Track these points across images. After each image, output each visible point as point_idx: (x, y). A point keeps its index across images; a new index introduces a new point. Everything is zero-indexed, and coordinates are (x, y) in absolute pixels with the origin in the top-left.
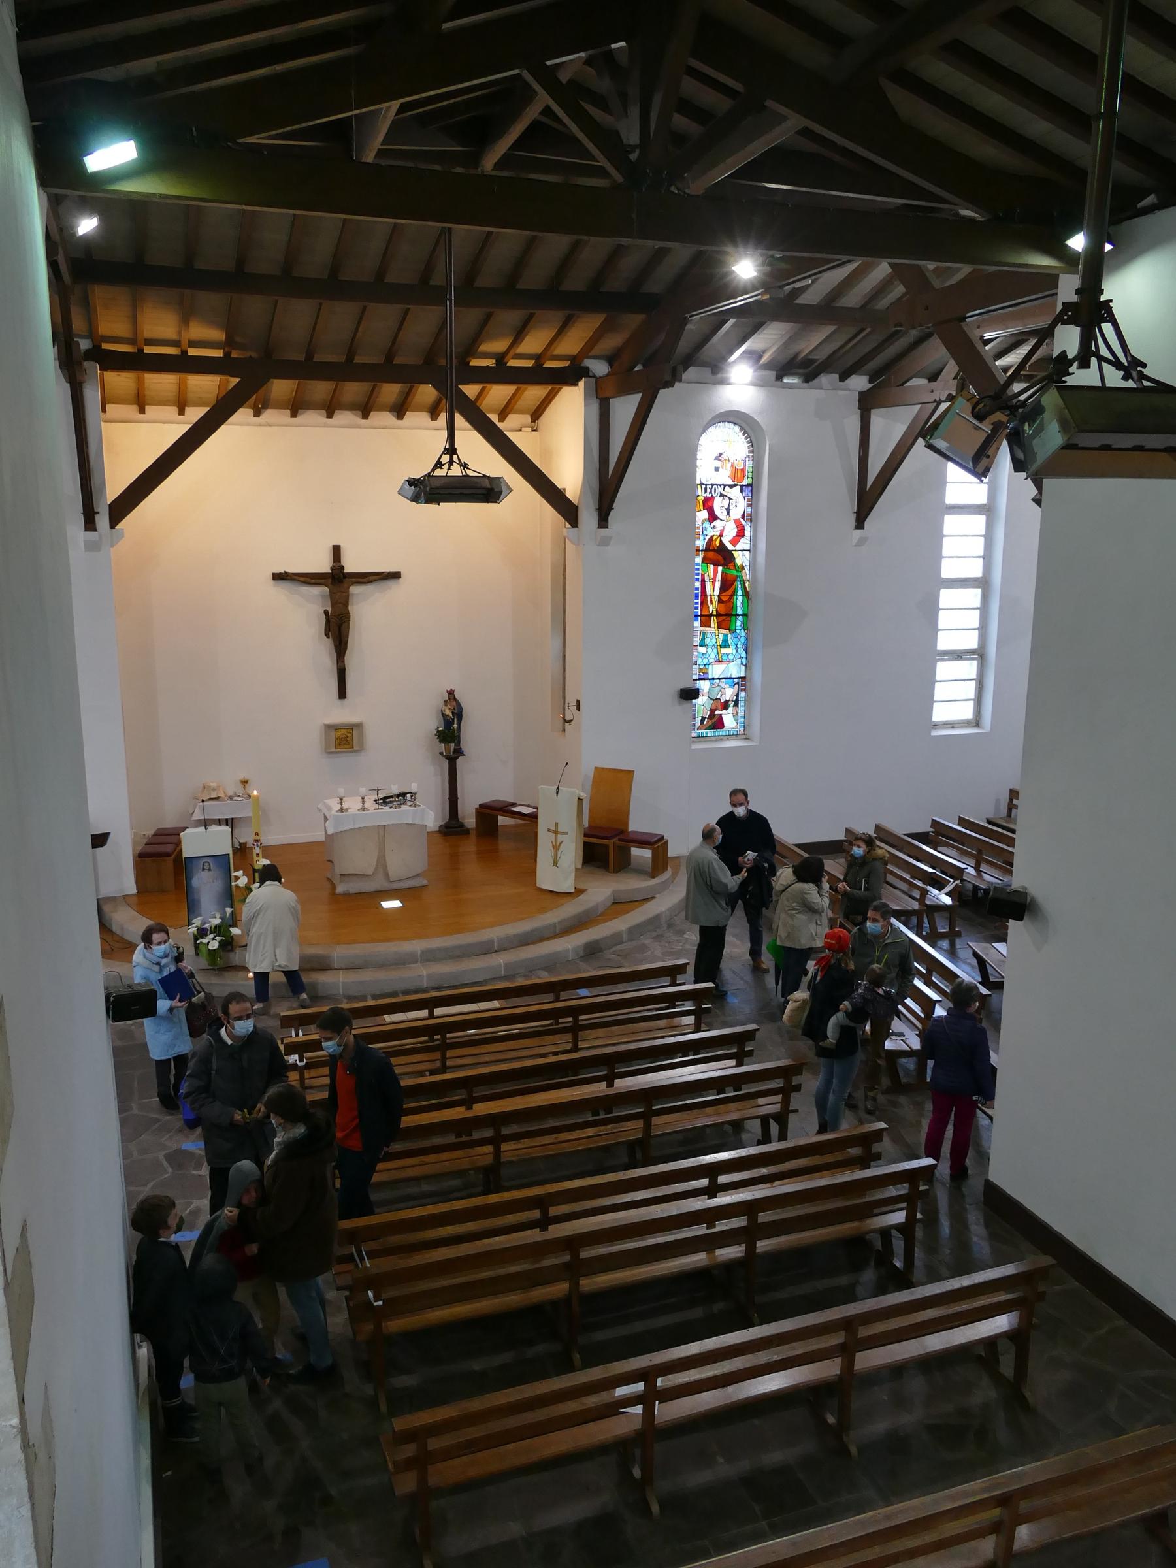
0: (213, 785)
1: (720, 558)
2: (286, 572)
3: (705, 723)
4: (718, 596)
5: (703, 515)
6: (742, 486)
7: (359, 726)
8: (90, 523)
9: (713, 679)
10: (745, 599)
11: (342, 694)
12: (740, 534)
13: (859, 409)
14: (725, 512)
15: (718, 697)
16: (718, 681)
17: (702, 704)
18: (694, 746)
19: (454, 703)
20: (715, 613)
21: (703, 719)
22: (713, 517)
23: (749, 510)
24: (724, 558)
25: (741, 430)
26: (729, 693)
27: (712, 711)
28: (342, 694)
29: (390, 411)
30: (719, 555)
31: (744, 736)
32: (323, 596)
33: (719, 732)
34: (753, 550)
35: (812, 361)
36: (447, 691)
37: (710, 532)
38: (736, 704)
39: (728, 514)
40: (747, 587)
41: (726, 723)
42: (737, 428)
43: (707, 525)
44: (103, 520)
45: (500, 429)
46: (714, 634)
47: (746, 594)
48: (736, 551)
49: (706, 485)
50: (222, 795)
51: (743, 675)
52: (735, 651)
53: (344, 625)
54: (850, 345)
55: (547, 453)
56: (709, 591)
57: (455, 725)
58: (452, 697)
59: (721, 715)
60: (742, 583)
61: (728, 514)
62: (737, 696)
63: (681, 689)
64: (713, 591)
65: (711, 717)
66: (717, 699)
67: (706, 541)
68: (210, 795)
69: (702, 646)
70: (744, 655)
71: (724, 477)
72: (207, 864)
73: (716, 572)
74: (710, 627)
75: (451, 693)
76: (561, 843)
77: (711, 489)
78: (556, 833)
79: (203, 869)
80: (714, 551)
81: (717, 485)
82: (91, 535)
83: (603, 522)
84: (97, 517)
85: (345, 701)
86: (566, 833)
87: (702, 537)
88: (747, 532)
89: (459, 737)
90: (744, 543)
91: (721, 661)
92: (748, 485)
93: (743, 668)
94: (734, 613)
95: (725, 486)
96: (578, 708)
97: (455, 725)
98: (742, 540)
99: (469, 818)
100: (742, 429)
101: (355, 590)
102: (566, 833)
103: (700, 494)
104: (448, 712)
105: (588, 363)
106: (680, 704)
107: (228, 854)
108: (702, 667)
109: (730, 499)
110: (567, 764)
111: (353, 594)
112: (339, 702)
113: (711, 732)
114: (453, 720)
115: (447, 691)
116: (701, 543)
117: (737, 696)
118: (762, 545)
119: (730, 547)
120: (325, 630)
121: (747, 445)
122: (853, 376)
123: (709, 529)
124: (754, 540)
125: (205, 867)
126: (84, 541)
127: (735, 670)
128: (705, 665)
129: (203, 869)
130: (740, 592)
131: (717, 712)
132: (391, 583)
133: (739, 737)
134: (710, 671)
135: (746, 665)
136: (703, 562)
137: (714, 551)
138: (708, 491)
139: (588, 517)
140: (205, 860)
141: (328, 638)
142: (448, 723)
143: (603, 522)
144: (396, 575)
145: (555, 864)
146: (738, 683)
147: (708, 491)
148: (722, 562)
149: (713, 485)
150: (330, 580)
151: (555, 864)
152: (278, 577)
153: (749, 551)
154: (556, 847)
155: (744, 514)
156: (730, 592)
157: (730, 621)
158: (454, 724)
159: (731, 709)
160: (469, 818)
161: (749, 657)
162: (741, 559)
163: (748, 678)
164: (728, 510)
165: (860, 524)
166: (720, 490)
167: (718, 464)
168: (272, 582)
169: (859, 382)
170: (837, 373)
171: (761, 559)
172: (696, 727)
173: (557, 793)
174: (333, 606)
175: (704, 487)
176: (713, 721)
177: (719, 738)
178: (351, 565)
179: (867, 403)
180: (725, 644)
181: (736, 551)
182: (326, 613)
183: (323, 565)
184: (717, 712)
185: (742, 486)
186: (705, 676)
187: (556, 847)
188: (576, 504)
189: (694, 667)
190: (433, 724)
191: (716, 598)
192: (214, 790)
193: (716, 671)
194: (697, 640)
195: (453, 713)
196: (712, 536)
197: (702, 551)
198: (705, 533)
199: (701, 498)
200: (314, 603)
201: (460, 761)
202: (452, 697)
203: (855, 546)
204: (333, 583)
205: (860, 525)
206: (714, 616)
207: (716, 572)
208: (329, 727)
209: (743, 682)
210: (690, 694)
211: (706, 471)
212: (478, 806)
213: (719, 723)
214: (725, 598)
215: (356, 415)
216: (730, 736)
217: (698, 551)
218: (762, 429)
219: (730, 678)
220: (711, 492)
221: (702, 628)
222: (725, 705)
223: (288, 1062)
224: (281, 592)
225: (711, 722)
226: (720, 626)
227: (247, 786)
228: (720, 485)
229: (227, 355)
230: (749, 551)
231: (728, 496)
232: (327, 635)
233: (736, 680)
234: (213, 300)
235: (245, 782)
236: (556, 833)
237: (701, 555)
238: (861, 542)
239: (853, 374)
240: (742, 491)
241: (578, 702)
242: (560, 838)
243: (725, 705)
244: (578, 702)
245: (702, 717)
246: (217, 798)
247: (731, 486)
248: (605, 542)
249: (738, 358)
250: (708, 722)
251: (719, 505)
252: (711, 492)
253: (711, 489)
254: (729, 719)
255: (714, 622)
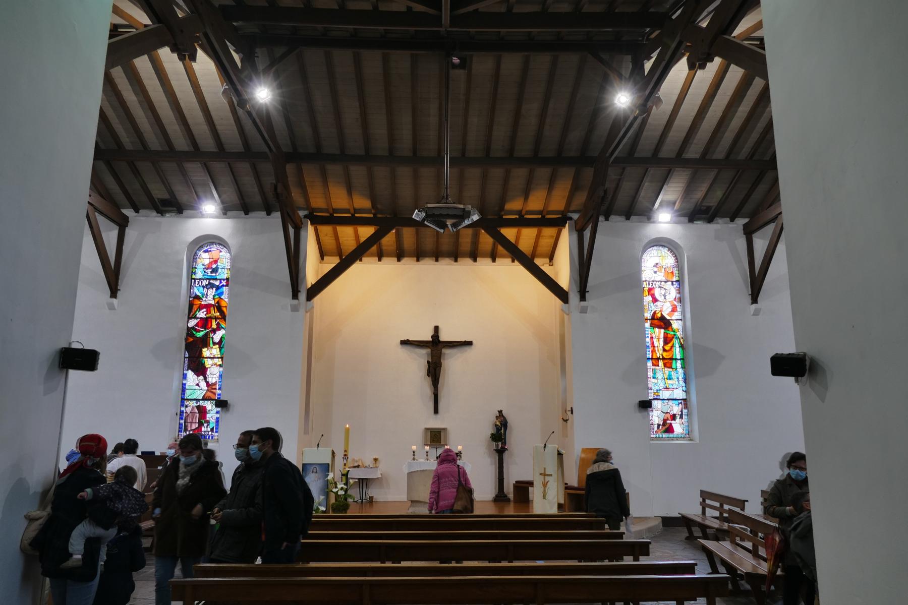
0: (356, 459)
1: (662, 324)
2: (407, 340)
3: (660, 428)
4: (663, 347)
5: (648, 299)
6: (672, 282)
7: (445, 429)
8: (295, 296)
9: (664, 399)
10: (681, 349)
11: (436, 411)
12: (674, 310)
13: (744, 234)
14: (663, 297)
15: (669, 411)
16: (667, 401)
17: (656, 416)
18: (651, 442)
19: (502, 418)
20: (661, 357)
21: (659, 425)
22: (655, 300)
23: (678, 296)
24: (665, 324)
25: (668, 250)
26: (676, 409)
27: (665, 421)
28: (436, 411)
29: (470, 257)
30: (662, 322)
31: (689, 439)
32: (428, 354)
33: (671, 435)
34: (683, 319)
35: (709, 208)
36: (498, 411)
37: (654, 307)
38: (681, 417)
39: (665, 298)
40: (682, 342)
41: (675, 429)
42: (666, 250)
43: (652, 304)
44: (303, 296)
45: (525, 254)
46: (661, 371)
47: (682, 346)
48: (672, 320)
49: (649, 281)
50: (360, 464)
51: (685, 397)
52: (677, 383)
53: (437, 369)
54: (728, 192)
55: (557, 274)
56: (656, 344)
57: (502, 431)
58: (501, 415)
59: (671, 424)
60: (678, 339)
61: (665, 298)
62: (682, 411)
63: (640, 401)
64: (660, 344)
65: (664, 424)
66: (667, 413)
67: (652, 314)
68: (354, 464)
69: (654, 378)
70: (684, 384)
71: (660, 276)
72: (315, 469)
73: (660, 333)
74: (658, 366)
75: (500, 412)
76: (547, 482)
77: (652, 284)
78: (544, 475)
79: (313, 472)
80: (657, 319)
81: (656, 281)
82: (295, 302)
83: (583, 298)
84: (299, 294)
85: (438, 416)
86: (551, 475)
87: (649, 312)
88: (679, 309)
89: (505, 439)
90: (677, 315)
91: (669, 388)
92: (676, 281)
93: (684, 393)
94: (674, 357)
95: (661, 281)
96: (572, 413)
97: (502, 431)
98: (676, 314)
99: (509, 489)
100: (669, 249)
101: (446, 351)
102: (551, 475)
103: (645, 286)
104: (498, 423)
105: (570, 215)
106: (640, 412)
107: (329, 464)
108: (655, 391)
109: (665, 289)
110: (553, 432)
111: (445, 354)
112: (434, 416)
113: (665, 435)
114: (501, 427)
115: (498, 411)
116: (648, 315)
117: (682, 411)
118: (688, 315)
119: (668, 318)
120: (428, 372)
121: (673, 258)
122: (736, 219)
123: (653, 307)
124: (683, 313)
125: (314, 471)
126: (291, 305)
127: (680, 394)
128: (657, 390)
129: (313, 472)
130: (677, 345)
131: (668, 422)
132: (467, 348)
133: (686, 439)
134: (661, 394)
135: (686, 391)
136: (651, 326)
137: (657, 319)
138: (651, 285)
139: (574, 297)
140: (315, 466)
141: (429, 376)
142: (498, 429)
143: (583, 298)
144: (469, 343)
145: (544, 497)
146: (681, 403)
147: (651, 285)
148: (663, 326)
149: (653, 281)
150: (431, 344)
151: (544, 497)
152: (405, 343)
153: (681, 320)
154: (545, 485)
155: (675, 298)
156: (670, 345)
157: (672, 363)
158: (501, 430)
159: (678, 420)
160: (509, 489)
161: (687, 386)
162: (675, 325)
163: (688, 400)
164: (665, 296)
165: (755, 300)
166: (658, 284)
167: (655, 269)
168: (400, 346)
169: (741, 221)
170: (728, 217)
171: (689, 324)
172: (654, 431)
173: (545, 447)
174: (432, 358)
175: (647, 282)
176: (666, 427)
177: (672, 439)
178: (444, 337)
179: (749, 232)
180: (670, 378)
181: (672, 320)
182: (428, 362)
183: (426, 335)
184: (668, 422)
185: (672, 282)
186: (658, 398)
187: (545, 485)
188: (567, 291)
189: (650, 391)
190: (490, 430)
191: (662, 348)
192: (357, 461)
193: (665, 394)
194: (650, 374)
195: (501, 424)
196: (656, 311)
197: (650, 319)
198: (650, 309)
199: (646, 289)
200: (421, 358)
201: (506, 455)
202: (501, 415)
203: (753, 315)
204: (433, 346)
205: (755, 300)
206: (661, 359)
207: (660, 333)
208: (427, 429)
209: (685, 402)
210: (645, 405)
211: (648, 273)
212: (515, 483)
213: (670, 430)
214: (667, 348)
215: (451, 259)
216: (677, 438)
217: (647, 319)
218: (681, 246)
219: (675, 399)
220: (652, 285)
221: (653, 367)
222: (674, 417)
223: (206, 444)
224: (404, 352)
225: (664, 428)
226: (665, 365)
227: (377, 462)
228: (658, 281)
229: (375, 215)
230: (681, 320)
231: (664, 287)
232: (428, 375)
233: (680, 401)
234: (358, 172)
235: (376, 460)
236: (544, 475)
237: (649, 322)
238: (756, 313)
239: (736, 218)
240: (673, 284)
241: (572, 408)
242: (547, 478)
243: (674, 417)
244: (572, 408)
245: (658, 424)
246: (358, 466)
247: (666, 282)
248: (584, 311)
249: (658, 207)
250: (662, 428)
251: (657, 293)
252: (652, 285)
253: (652, 284)
254: (678, 427)
255: (661, 363)
